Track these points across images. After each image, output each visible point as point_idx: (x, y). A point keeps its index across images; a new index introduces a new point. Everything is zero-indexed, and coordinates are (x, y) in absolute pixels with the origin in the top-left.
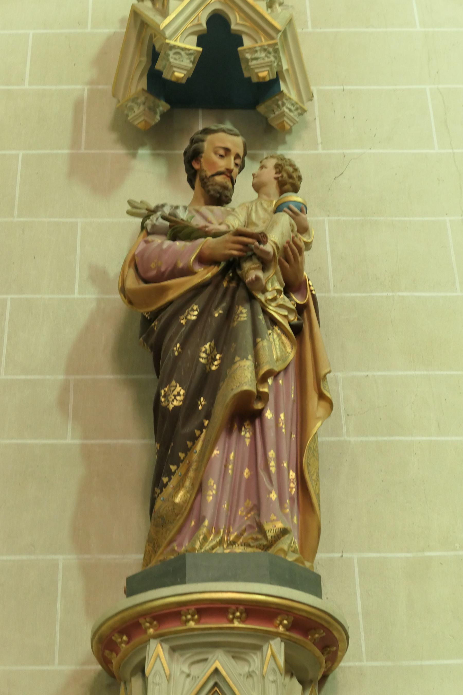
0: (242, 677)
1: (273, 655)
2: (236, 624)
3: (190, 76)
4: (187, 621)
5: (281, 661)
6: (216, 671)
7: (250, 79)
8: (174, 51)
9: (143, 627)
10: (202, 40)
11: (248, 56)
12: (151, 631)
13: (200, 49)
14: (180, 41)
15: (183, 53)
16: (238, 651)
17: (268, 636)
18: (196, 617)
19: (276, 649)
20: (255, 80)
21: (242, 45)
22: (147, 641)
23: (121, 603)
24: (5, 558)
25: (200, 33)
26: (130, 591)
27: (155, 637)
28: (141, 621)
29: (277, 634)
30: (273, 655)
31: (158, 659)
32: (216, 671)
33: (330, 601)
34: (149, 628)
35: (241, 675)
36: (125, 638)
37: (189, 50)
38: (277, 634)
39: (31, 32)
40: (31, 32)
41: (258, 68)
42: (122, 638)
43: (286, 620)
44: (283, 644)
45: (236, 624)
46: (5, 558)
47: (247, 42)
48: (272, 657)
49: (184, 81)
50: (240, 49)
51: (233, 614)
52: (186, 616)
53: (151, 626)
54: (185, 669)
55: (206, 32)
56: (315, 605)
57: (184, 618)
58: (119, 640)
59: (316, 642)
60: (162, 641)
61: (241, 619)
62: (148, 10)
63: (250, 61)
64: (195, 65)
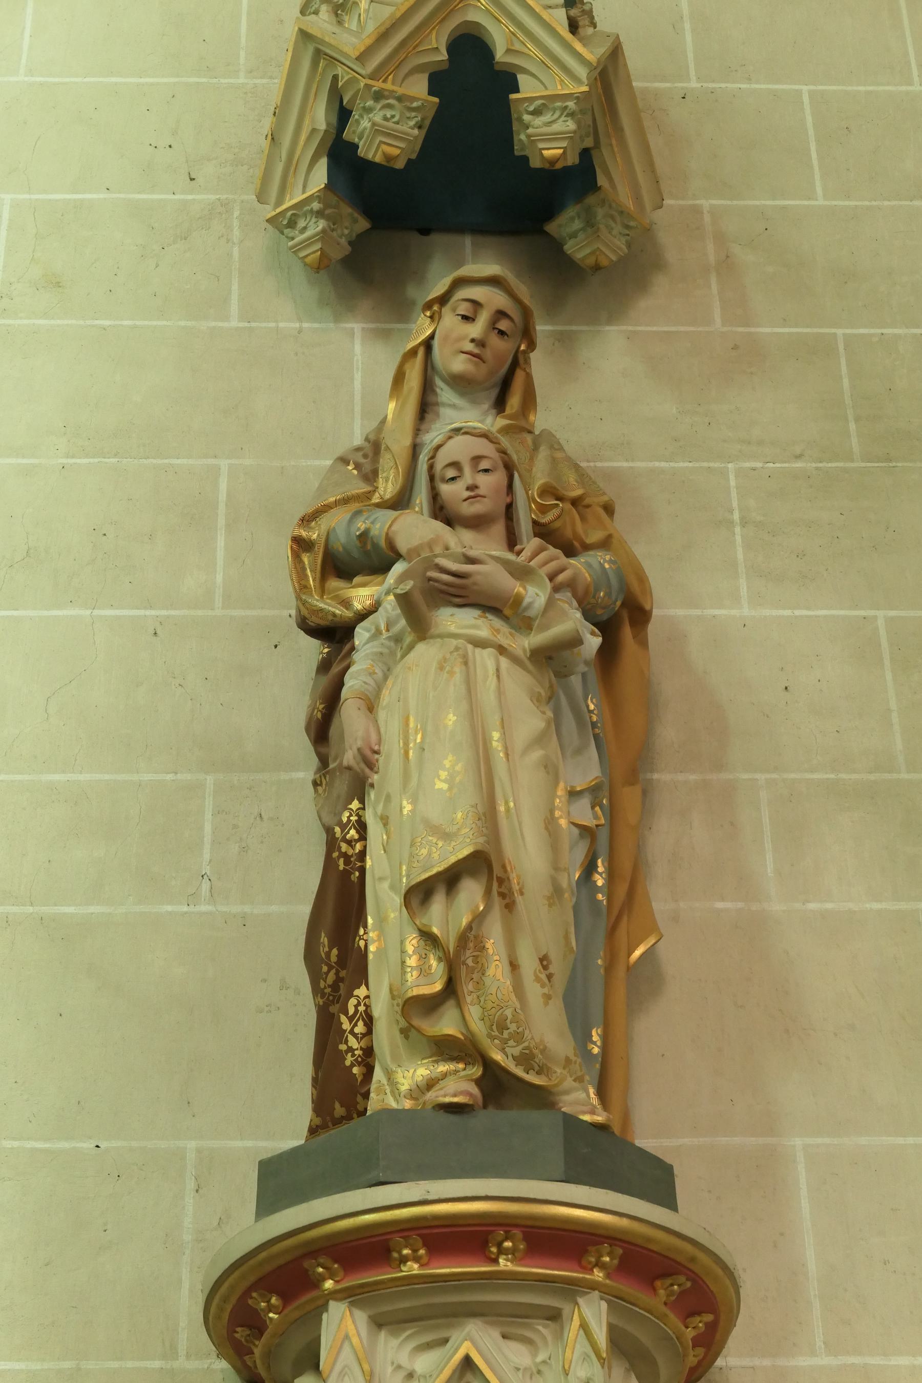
0: (520, 1374)
1: (584, 1326)
2: (504, 1264)
3: (414, 156)
4: (404, 1260)
5: (601, 1336)
6: (467, 1362)
7: (525, 159)
10: (438, 82)
12: (329, 1284)
13: (436, 100)
14: (393, 84)
16: (512, 1320)
17: (571, 1290)
19: (593, 1313)
20: (535, 163)
21: (518, 91)
22: (324, 1307)
23: (248, 1229)
25: (437, 69)
26: (268, 1203)
27: (335, 1295)
28: (306, 1264)
29: (594, 1286)
30: (584, 1326)
31: (346, 1344)
32: (467, 1362)
33: (697, 1216)
34: (323, 1279)
35: (518, 1369)
36: (274, 1300)
37: (414, 99)
38: (594, 1286)
42: (268, 1302)
43: (406, 1247)
44: (604, 1305)
47: (528, 88)
48: (581, 1332)
49: (400, 165)
50: (513, 96)
51: (499, 1245)
52: (400, 1252)
54: (403, 1357)
55: (446, 66)
57: (395, 1255)
59: (679, 1298)
60: (352, 1304)
62: (321, 21)
64: (424, 131)
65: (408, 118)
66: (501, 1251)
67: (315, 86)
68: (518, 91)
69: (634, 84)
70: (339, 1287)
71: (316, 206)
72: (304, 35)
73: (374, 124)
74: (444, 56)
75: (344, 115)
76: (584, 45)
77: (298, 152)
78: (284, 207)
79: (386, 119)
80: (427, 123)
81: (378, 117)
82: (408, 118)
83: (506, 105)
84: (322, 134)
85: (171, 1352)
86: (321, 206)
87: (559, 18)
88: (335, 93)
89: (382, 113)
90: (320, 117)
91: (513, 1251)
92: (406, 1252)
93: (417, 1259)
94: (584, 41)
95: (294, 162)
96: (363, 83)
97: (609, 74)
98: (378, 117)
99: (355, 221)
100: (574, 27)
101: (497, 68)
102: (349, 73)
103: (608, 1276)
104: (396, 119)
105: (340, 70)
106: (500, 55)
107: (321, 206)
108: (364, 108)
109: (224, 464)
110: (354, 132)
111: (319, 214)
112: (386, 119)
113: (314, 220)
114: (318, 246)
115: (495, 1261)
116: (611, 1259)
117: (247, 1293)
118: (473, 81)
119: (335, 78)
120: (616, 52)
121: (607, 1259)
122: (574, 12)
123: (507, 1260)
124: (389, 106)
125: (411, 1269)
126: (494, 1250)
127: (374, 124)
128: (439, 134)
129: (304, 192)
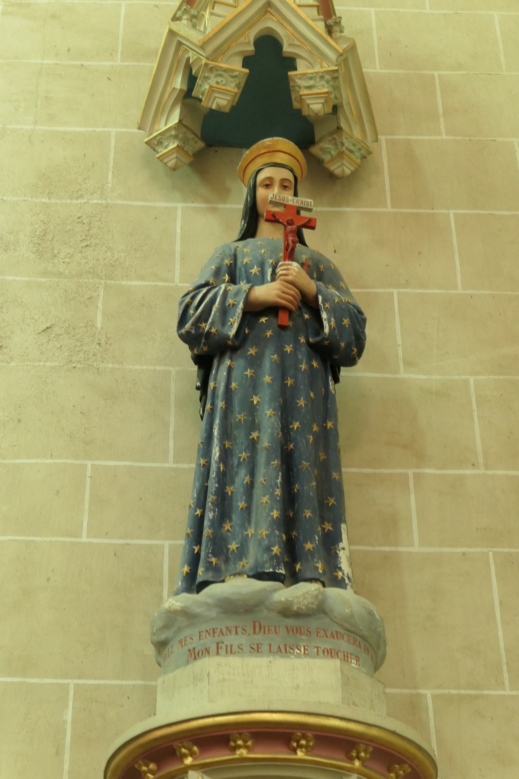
2: (243, 752)
3: (235, 104)
8: (215, 73)
9: (178, 754)
11: (302, 83)
12: (189, 761)
13: (247, 71)
15: (225, 75)
18: (249, 743)
21: (295, 69)
24: (5, 679)
28: (176, 744)
34: (185, 756)
37: (233, 71)
39: (114, 131)
40: (114, 131)
41: (347, 156)
45: (243, 752)
46: (5, 679)
47: (302, 67)
51: (298, 742)
52: (235, 742)
53: (192, 754)
55: (253, 53)
56: (391, 727)
57: (232, 744)
58: (144, 768)
61: (308, 749)
63: (303, 88)
64: (241, 90)
65: (231, 82)
66: (300, 746)
67: (176, 64)
68: (295, 69)
69: (364, 70)
70: (197, 762)
71: (173, 133)
72: (172, 33)
73: (211, 87)
74: (252, 48)
75: (192, 80)
76: (337, 43)
77: (165, 99)
78: (155, 134)
79: (217, 83)
80: (242, 84)
81: (213, 84)
82: (231, 82)
83: (286, 79)
84: (178, 90)
85: (417, 476)
86: (176, 132)
87: (320, 27)
88: (188, 67)
89: (215, 80)
90: (179, 83)
91: (306, 747)
92: (240, 742)
93: (247, 747)
94: (336, 40)
95: (163, 103)
96: (204, 61)
97: (349, 57)
98: (213, 82)
99: (196, 143)
100: (330, 30)
101: (285, 55)
102: (195, 55)
103: (363, 765)
104: (224, 83)
105: (191, 54)
106: (286, 49)
107: (176, 132)
108: (204, 77)
109: (71, 682)
110: (199, 92)
111: (176, 137)
112: (217, 83)
113: (172, 141)
114: (175, 155)
115: (294, 751)
116: (366, 754)
117: (135, 760)
118: (269, 61)
119: (188, 59)
120: (353, 48)
121: (363, 754)
122: (330, 22)
123: (302, 751)
124: (221, 75)
125: (242, 754)
126: (295, 744)
127: (211, 87)
128: (250, 90)
129: (166, 125)
